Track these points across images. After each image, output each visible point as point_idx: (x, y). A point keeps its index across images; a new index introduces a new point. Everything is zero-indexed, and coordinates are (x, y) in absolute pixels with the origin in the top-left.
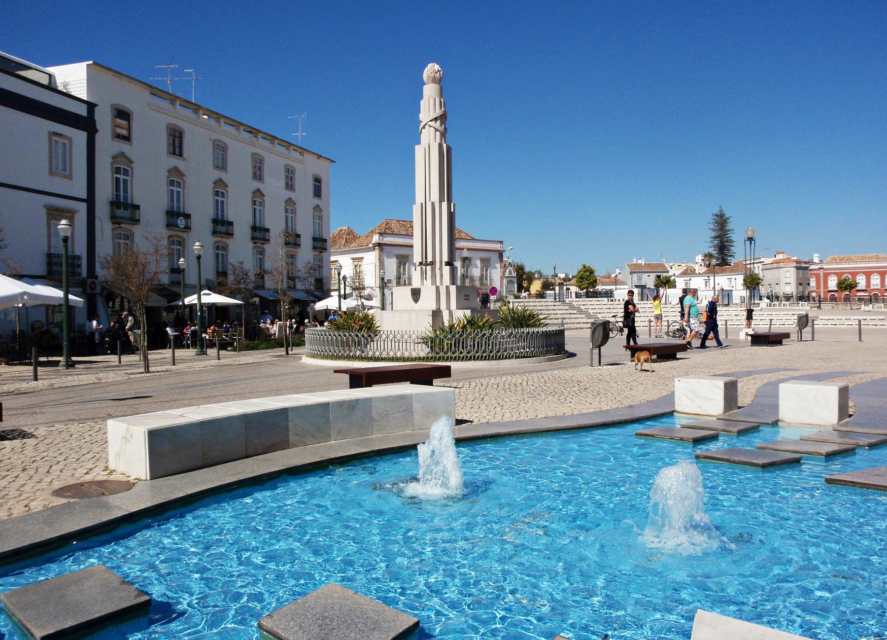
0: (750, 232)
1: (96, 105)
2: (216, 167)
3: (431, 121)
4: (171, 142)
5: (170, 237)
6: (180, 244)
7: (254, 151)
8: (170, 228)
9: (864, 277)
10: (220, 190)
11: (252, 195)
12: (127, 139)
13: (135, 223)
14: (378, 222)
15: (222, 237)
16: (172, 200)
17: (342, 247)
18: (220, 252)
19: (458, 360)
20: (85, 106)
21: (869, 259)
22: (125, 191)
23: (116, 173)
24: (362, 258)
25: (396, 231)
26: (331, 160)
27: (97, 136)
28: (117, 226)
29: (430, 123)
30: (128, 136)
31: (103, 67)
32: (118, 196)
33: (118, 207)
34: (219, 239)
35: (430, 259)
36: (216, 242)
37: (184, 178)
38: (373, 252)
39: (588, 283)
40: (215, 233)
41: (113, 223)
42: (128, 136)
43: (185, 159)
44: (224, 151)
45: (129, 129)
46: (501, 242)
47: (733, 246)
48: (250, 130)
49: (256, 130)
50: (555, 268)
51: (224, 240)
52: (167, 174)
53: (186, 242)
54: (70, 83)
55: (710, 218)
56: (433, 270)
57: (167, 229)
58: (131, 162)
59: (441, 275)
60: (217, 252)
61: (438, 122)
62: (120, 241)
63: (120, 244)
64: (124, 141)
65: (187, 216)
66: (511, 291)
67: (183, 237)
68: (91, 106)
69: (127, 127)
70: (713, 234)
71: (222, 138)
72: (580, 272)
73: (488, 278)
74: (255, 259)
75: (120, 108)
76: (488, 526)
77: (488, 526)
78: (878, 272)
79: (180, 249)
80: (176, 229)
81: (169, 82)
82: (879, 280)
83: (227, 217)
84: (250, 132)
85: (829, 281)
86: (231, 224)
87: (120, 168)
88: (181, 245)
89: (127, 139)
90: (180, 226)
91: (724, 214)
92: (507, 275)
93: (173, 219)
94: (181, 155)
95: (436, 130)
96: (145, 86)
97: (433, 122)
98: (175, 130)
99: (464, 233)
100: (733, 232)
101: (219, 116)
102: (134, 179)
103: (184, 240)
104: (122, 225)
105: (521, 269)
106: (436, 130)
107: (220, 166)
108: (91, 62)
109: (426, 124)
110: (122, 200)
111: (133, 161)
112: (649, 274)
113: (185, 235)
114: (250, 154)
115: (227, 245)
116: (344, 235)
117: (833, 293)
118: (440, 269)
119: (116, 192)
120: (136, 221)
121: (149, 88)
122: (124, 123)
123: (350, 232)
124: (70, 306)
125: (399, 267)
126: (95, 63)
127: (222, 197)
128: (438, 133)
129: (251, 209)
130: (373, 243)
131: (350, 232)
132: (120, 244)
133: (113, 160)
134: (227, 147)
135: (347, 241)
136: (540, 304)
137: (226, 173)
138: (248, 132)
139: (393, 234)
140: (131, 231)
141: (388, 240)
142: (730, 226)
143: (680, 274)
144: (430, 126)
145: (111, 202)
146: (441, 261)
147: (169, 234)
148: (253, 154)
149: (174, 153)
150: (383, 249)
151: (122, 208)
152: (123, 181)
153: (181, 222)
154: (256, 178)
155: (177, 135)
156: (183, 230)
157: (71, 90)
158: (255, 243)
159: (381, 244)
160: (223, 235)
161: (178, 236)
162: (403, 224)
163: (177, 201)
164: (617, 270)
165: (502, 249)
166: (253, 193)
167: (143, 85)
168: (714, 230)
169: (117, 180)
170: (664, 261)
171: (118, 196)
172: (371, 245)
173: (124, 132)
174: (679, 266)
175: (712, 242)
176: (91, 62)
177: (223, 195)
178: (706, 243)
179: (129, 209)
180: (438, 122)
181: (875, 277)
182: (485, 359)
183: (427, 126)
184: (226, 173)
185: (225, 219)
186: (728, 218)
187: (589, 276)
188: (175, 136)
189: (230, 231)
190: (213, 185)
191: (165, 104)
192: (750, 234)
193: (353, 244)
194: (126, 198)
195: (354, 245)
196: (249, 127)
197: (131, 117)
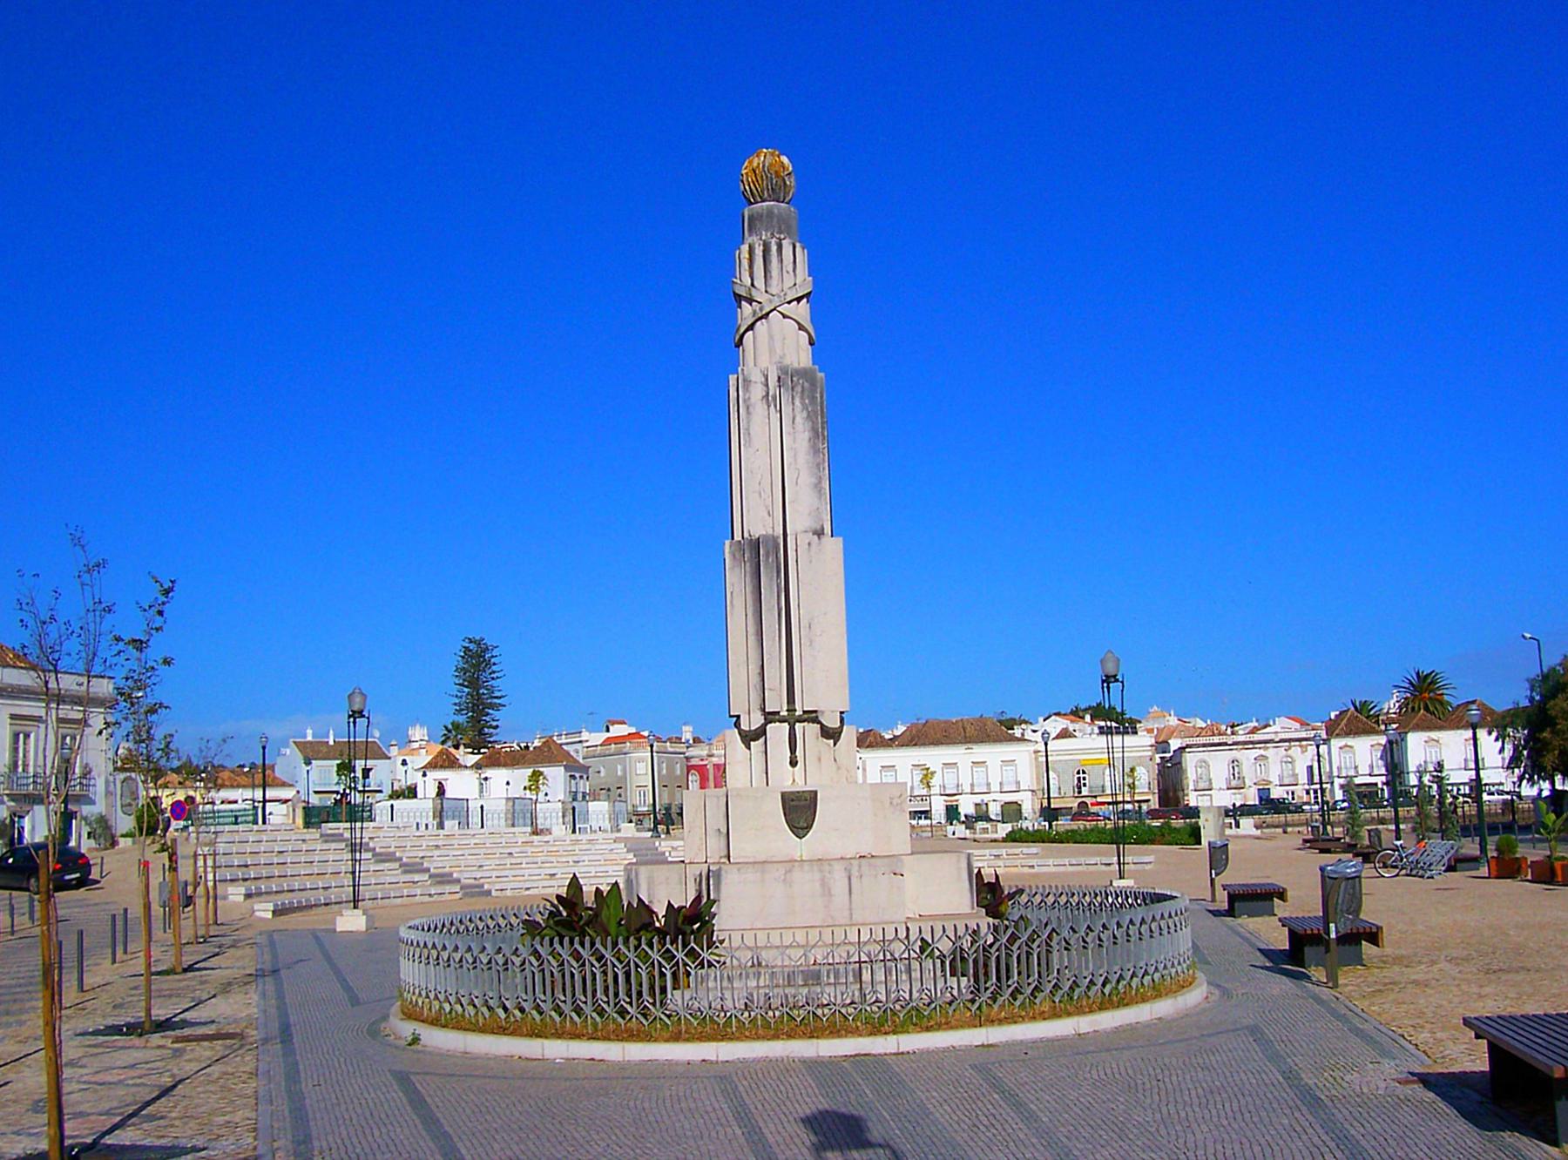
178: (446, 702)
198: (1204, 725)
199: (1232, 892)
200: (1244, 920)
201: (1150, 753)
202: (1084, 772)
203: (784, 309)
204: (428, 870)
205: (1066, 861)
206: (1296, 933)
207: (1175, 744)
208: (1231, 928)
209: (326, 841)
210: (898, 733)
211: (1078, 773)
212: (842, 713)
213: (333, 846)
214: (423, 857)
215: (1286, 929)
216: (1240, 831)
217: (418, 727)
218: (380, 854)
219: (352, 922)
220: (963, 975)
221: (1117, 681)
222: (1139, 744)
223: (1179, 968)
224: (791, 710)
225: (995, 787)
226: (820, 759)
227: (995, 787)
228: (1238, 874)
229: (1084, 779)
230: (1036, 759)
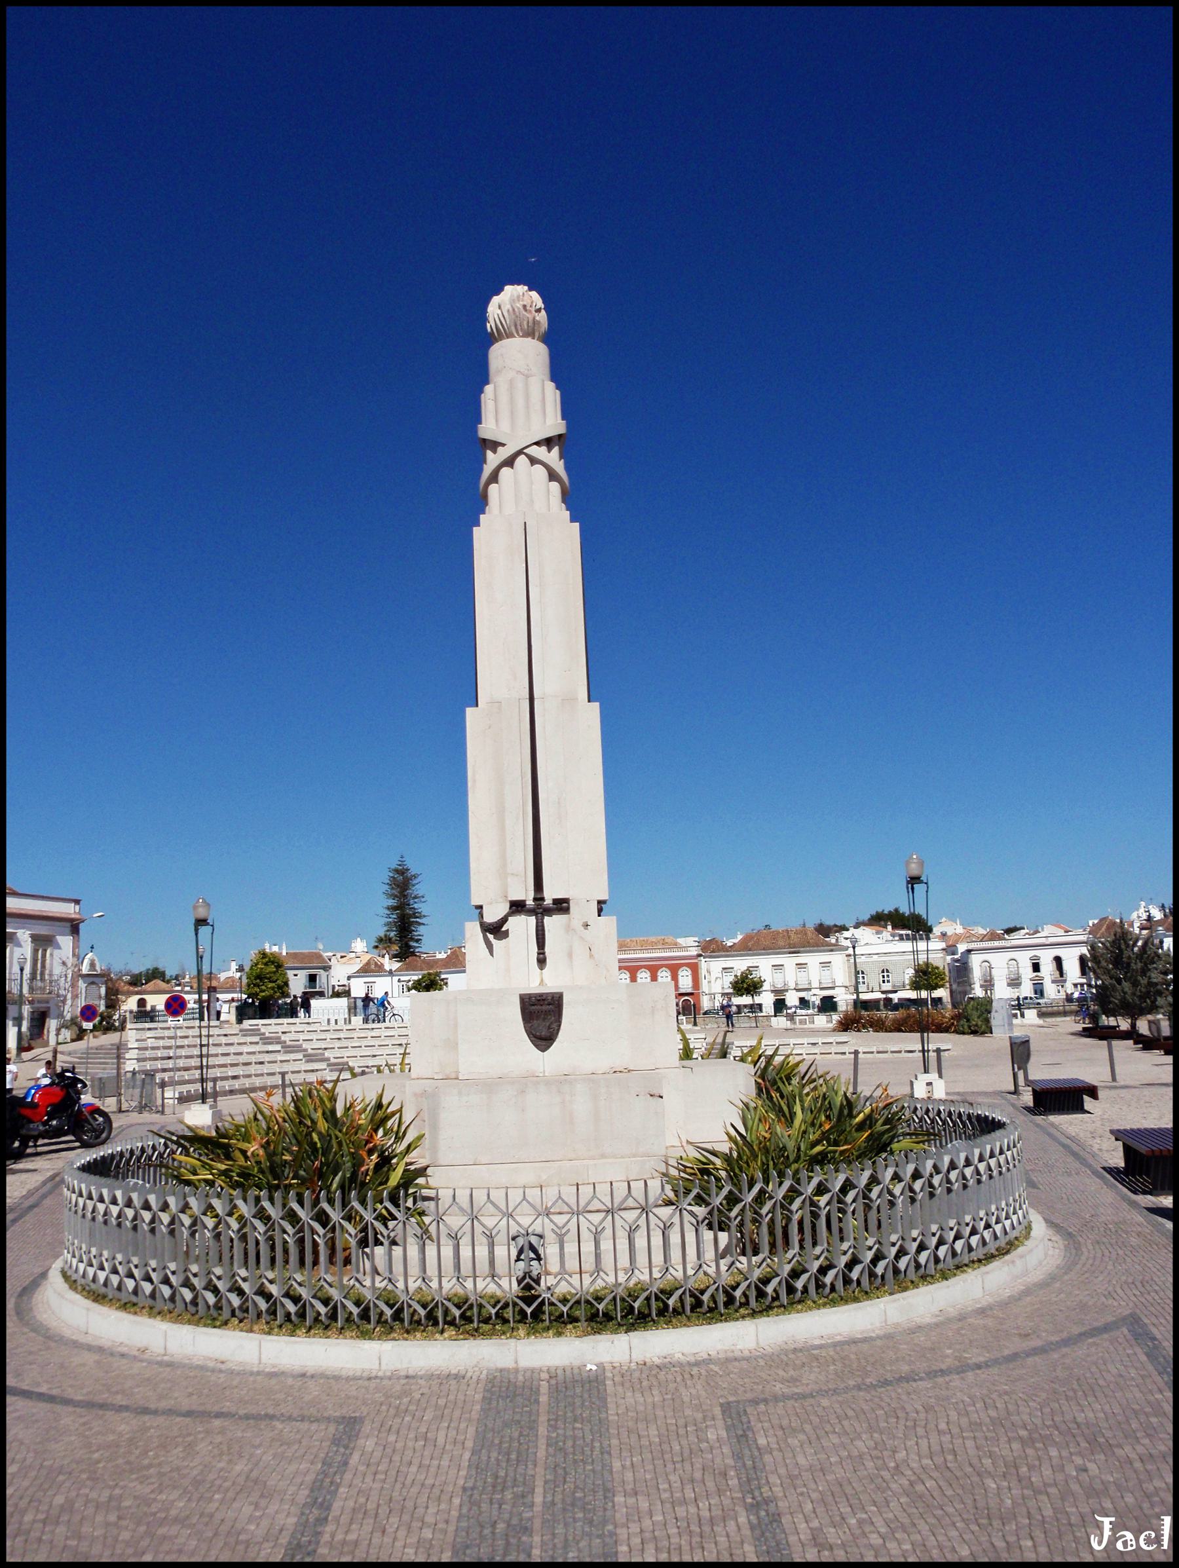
0: (913, 866)
3: (537, 443)
9: (689, 973)
21: (653, 946)
39: (273, 988)
46: (77, 902)
47: (420, 924)
55: (386, 876)
61: (556, 450)
70: (392, 902)
72: (256, 965)
73: (47, 977)
76: (1154, 1420)
77: (1154, 1420)
78: (687, 965)
82: (690, 978)
85: (680, 977)
91: (408, 870)
92: (85, 969)
100: (423, 900)
109: (520, 452)
112: (296, 972)
117: (686, 998)
142: (419, 888)
143: (357, 972)
144: (533, 461)
164: (1143, 904)
165: (77, 916)
168: (394, 896)
170: (321, 947)
174: (342, 957)
175: (388, 916)
178: (379, 922)
180: (556, 450)
181: (685, 973)
183: (522, 460)
186: (415, 876)
187: (274, 972)
192: (914, 870)
198: (985, 933)
199: (1038, 1089)
200: (1054, 1119)
201: (942, 955)
202: (888, 971)
203: (536, 451)
204: (328, 1059)
205: (874, 1049)
206: (1136, 1151)
207: (962, 948)
208: (1038, 1125)
209: (244, 1035)
210: (736, 941)
211: (883, 972)
212: (599, 902)
213: (249, 1039)
214: (326, 1049)
215: (1120, 1143)
216: (1026, 1021)
217: (359, 939)
218: (289, 1047)
219: (31, 1144)
220: (721, 1229)
221: (922, 882)
222: (936, 945)
223: (1008, 1223)
224: (539, 899)
225: (815, 984)
226: (570, 955)
227: (815, 984)
228: (1042, 1071)
229: (888, 976)
230: (848, 960)
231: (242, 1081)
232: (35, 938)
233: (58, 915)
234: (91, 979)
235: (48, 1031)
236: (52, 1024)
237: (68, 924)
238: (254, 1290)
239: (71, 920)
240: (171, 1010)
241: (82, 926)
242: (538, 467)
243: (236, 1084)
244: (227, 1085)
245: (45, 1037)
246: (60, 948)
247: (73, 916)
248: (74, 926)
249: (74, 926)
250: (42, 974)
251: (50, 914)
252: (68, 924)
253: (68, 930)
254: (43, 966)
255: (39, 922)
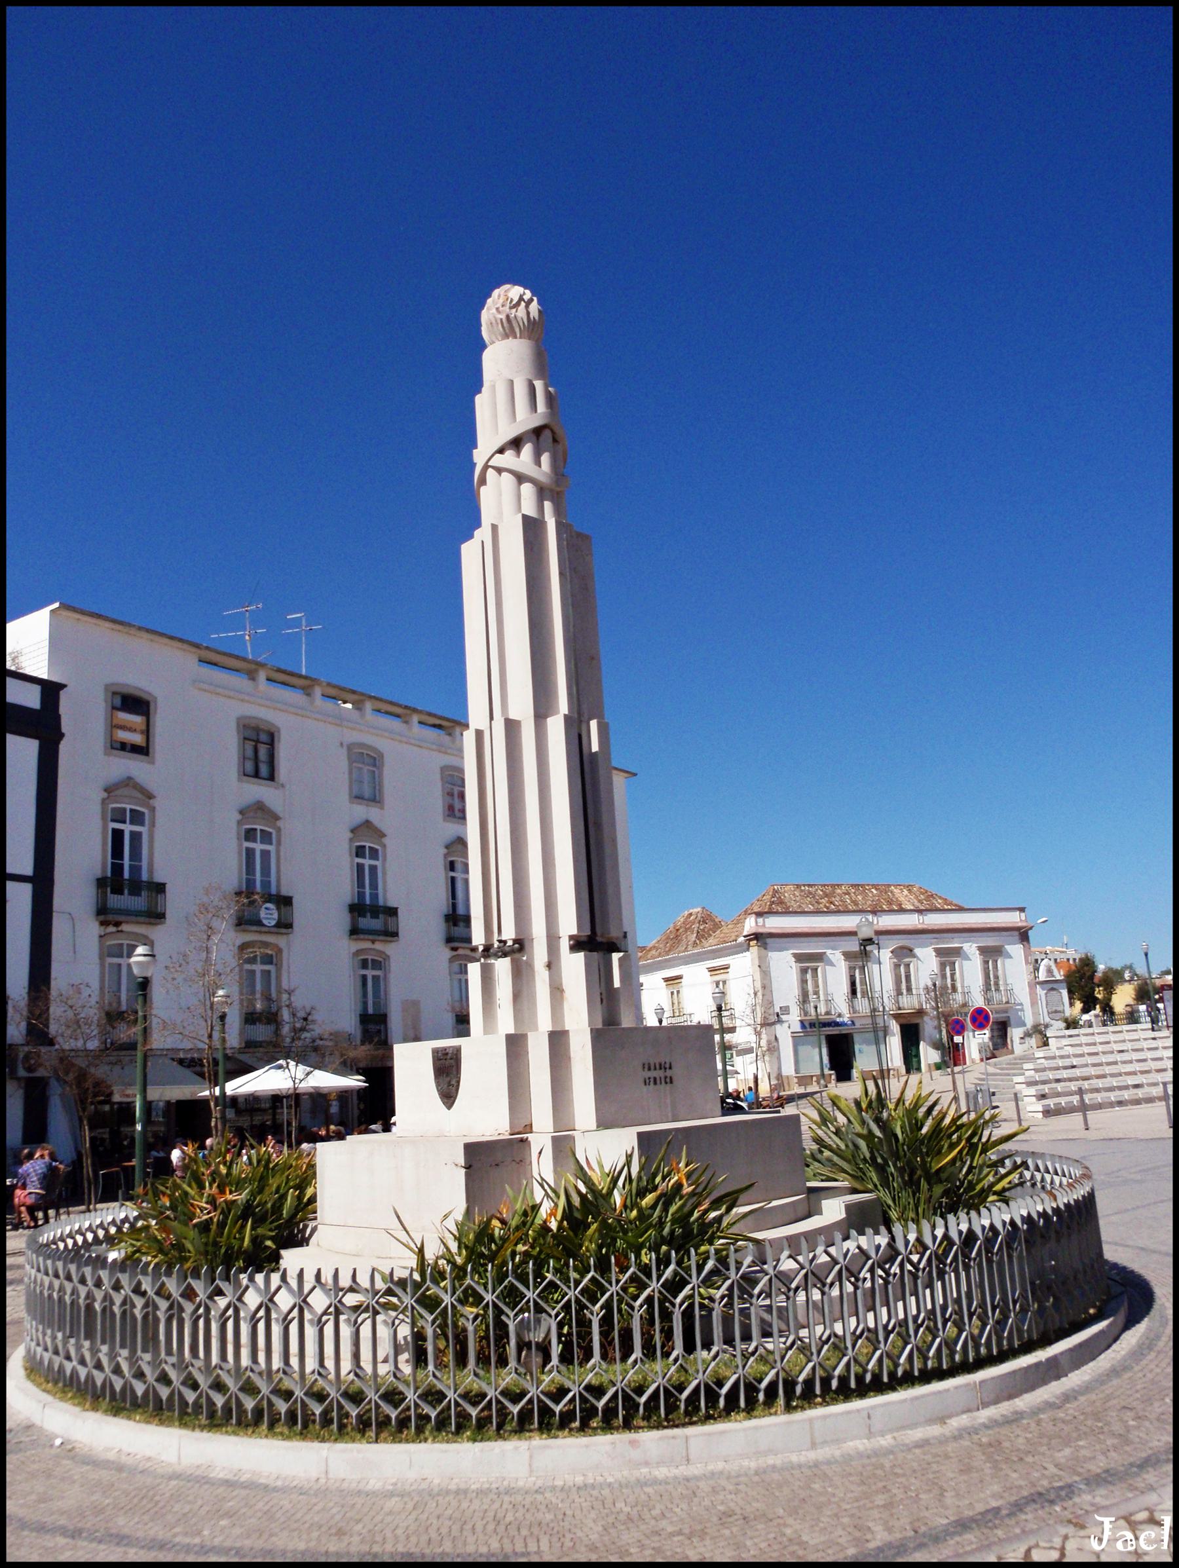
1: (62, 686)
2: (358, 798)
3: (501, 451)
4: (250, 753)
5: (243, 947)
6: (268, 960)
7: (443, 763)
8: (355, 937)
10: (368, 845)
11: (444, 851)
12: (375, 799)
13: (152, 920)
14: (759, 894)
15: (373, 942)
16: (360, 883)
17: (690, 948)
18: (370, 973)
19: (460, 1429)
20: (36, 690)
22: (374, 886)
23: (357, 856)
24: (726, 967)
25: (794, 906)
26: (627, 772)
27: (64, 747)
28: (111, 929)
29: (498, 461)
30: (144, 745)
31: (83, 612)
32: (361, 895)
33: (118, 891)
34: (368, 945)
35: (509, 933)
36: (358, 952)
37: (279, 823)
38: (747, 954)
40: (354, 932)
41: (103, 923)
42: (144, 745)
43: (283, 786)
44: (375, 765)
45: (147, 732)
46: (1022, 910)
48: (438, 722)
49: (448, 720)
50: (1146, 955)
51: (378, 946)
52: (239, 817)
53: (285, 955)
54: (24, 652)
56: (521, 974)
57: (236, 931)
58: (150, 796)
59: (557, 990)
60: (364, 972)
61: (527, 450)
62: (254, 967)
63: (253, 972)
64: (135, 756)
65: (285, 902)
66: (1056, 1012)
67: (277, 946)
68: (51, 690)
69: (144, 727)
71: (369, 739)
73: (1002, 988)
74: (456, 984)
75: (125, 691)
79: (269, 972)
80: (254, 928)
81: (247, 638)
83: (385, 899)
84: (439, 727)
86: (393, 912)
87: (364, 847)
88: (271, 963)
89: (142, 750)
90: (265, 922)
93: (456, 928)
94: (271, 777)
95: (520, 478)
96: (185, 646)
97: (509, 454)
98: (257, 730)
99: (940, 898)
101: (362, 698)
102: (282, 848)
103: (280, 951)
104: (124, 927)
105: (1087, 965)
106: (520, 478)
107: (367, 795)
108: (56, 605)
109: (486, 467)
110: (368, 901)
111: (155, 793)
113: (281, 941)
114: (438, 771)
115: (387, 958)
116: (694, 923)
118: (549, 966)
119: (113, 857)
120: (392, 934)
121: (194, 650)
122: (137, 720)
123: (706, 918)
124: (150, 1103)
125: (804, 982)
126: (65, 606)
127: (371, 858)
128: (527, 489)
129: (348, 866)
130: (745, 933)
131: (706, 918)
132: (253, 972)
133: (105, 795)
134: (381, 756)
135: (701, 936)
136: (1134, 1036)
137: (382, 808)
138: (434, 726)
139: (787, 912)
140: (384, 953)
141: (774, 924)
144: (499, 470)
145: (98, 880)
146: (552, 939)
147: (239, 942)
148: (443, 769)
149: (257, 775)
150: (766, 944)
151: (368, 915)
152: (262, 856)
153: (269, 914)
154: (454, 816)
155: (264, 737)
156: (275, 930)
157: (23, 665)
158: (454, 949)
159: (762, 934)
160: (376, 937)
161: (266, 945)
162: (810, 893)
163: (371, 885)
165: (1024, 924)
166: (447, 847)
167: (179, 644)
169: (250, 853)
171: (361, 895)
172: (741, 939)
173: (137, 739)
176: (56, 605)
177: (374, 854)
179: (381, 916)
180: (527, 450)
182: (608, 1425)
184: (382, 808)
185: (381, 903)
188: (257, 741)
189: (391, 928)
190: (350, 835)
191: (238, 682)
193: (711, 941)
194: (375, 896)
195: (711, 943)
196: (430, 714)
197: (276, 739)
203: (498, 461)
231: (1146, 1089)
232: (983, 951)
233: (1004, 925)
234: (1051, 986)
235: (1012, 1041)
236: (1015, 1033)
237: (1016, 933)
238: (209, 1383)
239: (1018, 929)
240: (977, 1024)
241: (1030, 933)
242: (504, 474)
243: (1140, 1093)
244: (1099, 1098)
245: (1010, 1047)
246: (1010, 957)
247: (1020, 924)
248: (1023, 935)
249: (1023, 935)
250: (997, 984)
251: (995, 925)
252: (1016, 933)
253: (1017, 938)
254: (996, 977)
255: (985, 934)
